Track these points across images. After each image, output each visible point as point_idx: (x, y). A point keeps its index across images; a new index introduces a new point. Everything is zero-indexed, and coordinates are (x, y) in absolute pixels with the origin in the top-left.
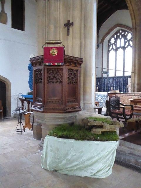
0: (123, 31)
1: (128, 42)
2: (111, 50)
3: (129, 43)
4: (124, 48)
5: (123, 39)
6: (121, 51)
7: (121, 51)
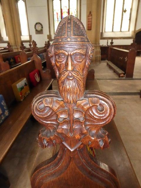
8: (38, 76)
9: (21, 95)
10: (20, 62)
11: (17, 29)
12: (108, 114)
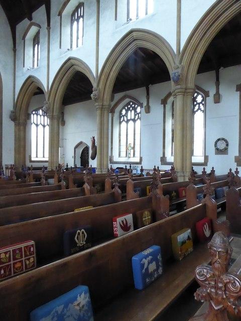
0: (133, 103)
1: (197, 106)
2: (197, 111)
3: (199, 107)
4: (134, 120)
6: (131, 123)
7: (131, 123)
8: (208, 228)
9: (181, 251)
10: (185, 196)
11: (188, 146)
12: (239, 290)
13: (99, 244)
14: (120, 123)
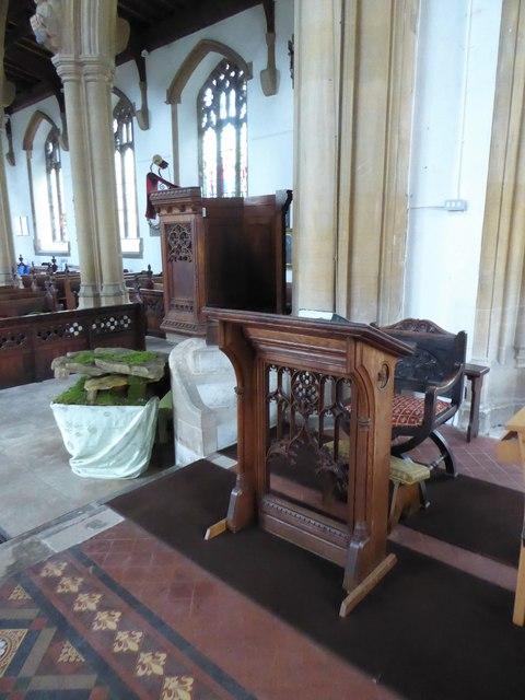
2: (206, 128)
4: (238, 122)
5: (233, 93)
7: (229, 130)
13: (116, 197)
14: (201, 132)
